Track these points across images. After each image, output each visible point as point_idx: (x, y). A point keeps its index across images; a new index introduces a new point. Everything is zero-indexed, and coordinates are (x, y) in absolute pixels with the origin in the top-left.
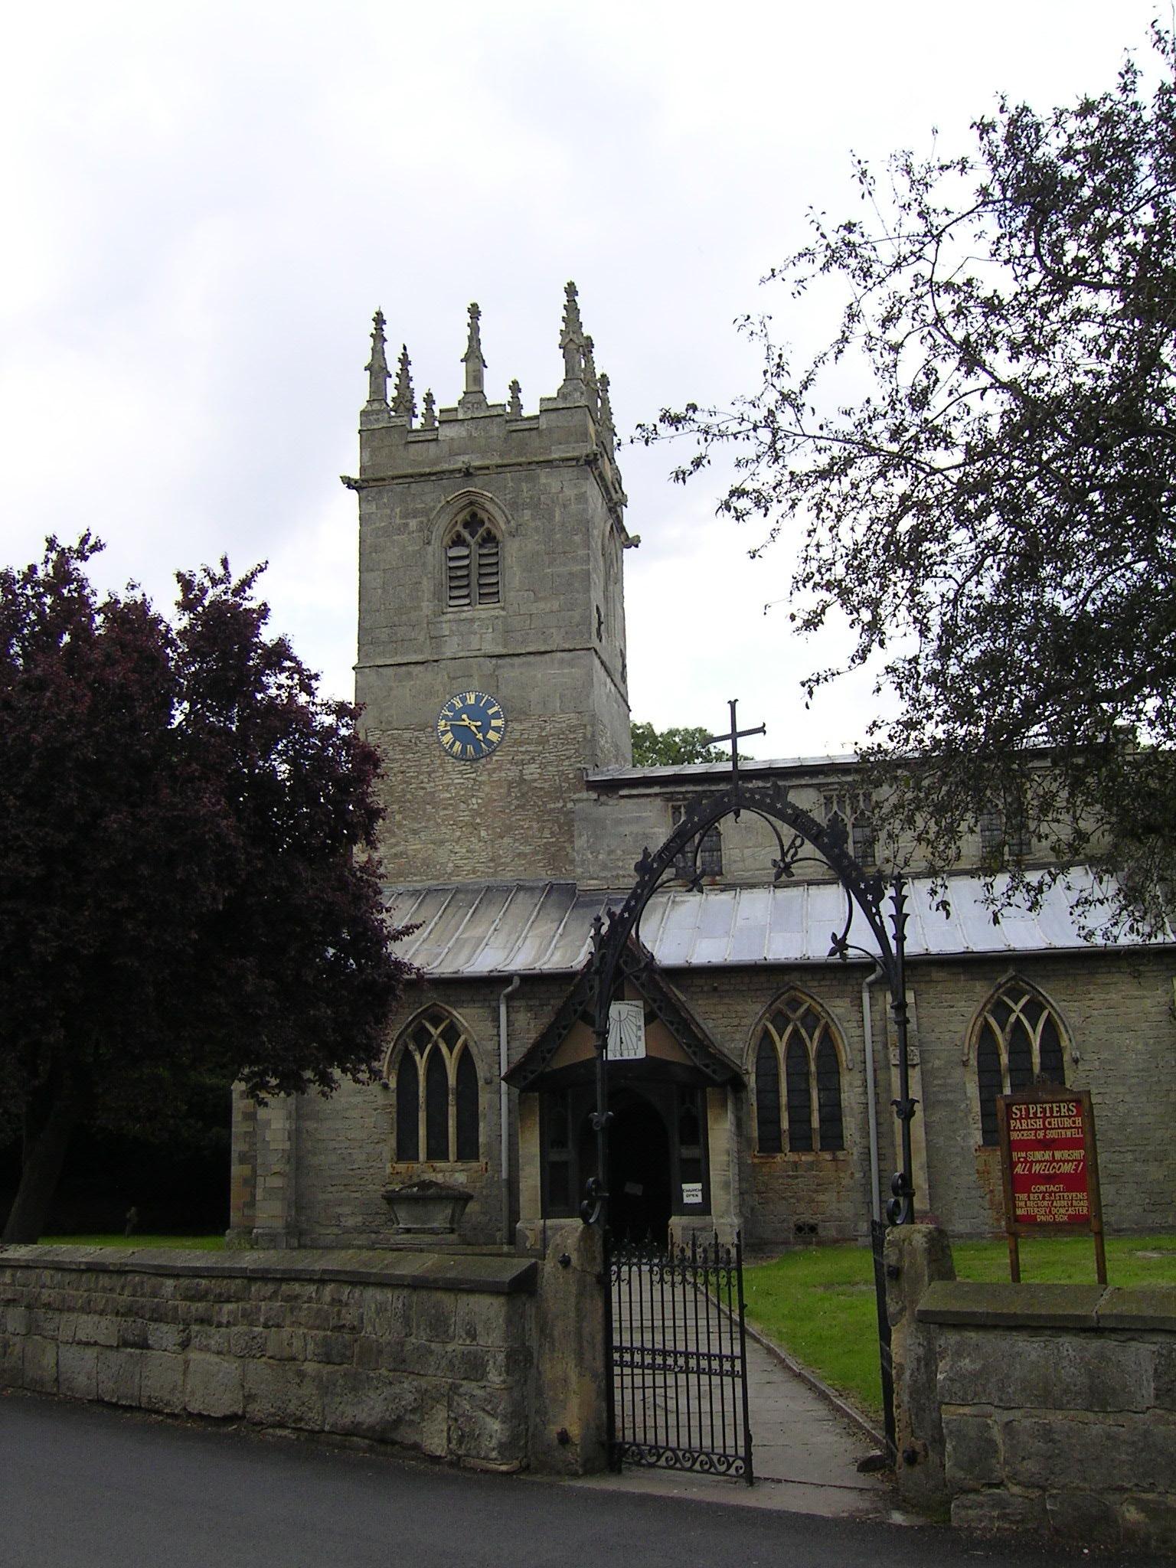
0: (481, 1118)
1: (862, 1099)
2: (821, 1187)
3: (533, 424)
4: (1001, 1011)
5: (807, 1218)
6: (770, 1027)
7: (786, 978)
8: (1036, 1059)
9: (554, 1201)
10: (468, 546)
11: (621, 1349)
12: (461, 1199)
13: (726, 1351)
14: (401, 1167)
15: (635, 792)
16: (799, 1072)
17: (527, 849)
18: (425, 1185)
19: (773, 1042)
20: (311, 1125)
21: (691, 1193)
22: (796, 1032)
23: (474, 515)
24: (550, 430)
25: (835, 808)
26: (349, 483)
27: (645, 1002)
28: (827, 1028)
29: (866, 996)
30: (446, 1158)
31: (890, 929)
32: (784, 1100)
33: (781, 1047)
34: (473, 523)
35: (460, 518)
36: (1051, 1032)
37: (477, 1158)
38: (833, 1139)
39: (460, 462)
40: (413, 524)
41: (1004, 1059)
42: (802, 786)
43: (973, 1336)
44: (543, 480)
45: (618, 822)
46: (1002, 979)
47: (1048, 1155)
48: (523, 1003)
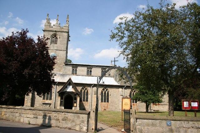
9: (61, 105)
12: (50, 104)
16: (84, 94)
21: (75, 105)
22: (84, 90)
37: (51, 100)
38: (87, 101)
39: (55, 30)
43: (141, 120)
45: (67, 68)
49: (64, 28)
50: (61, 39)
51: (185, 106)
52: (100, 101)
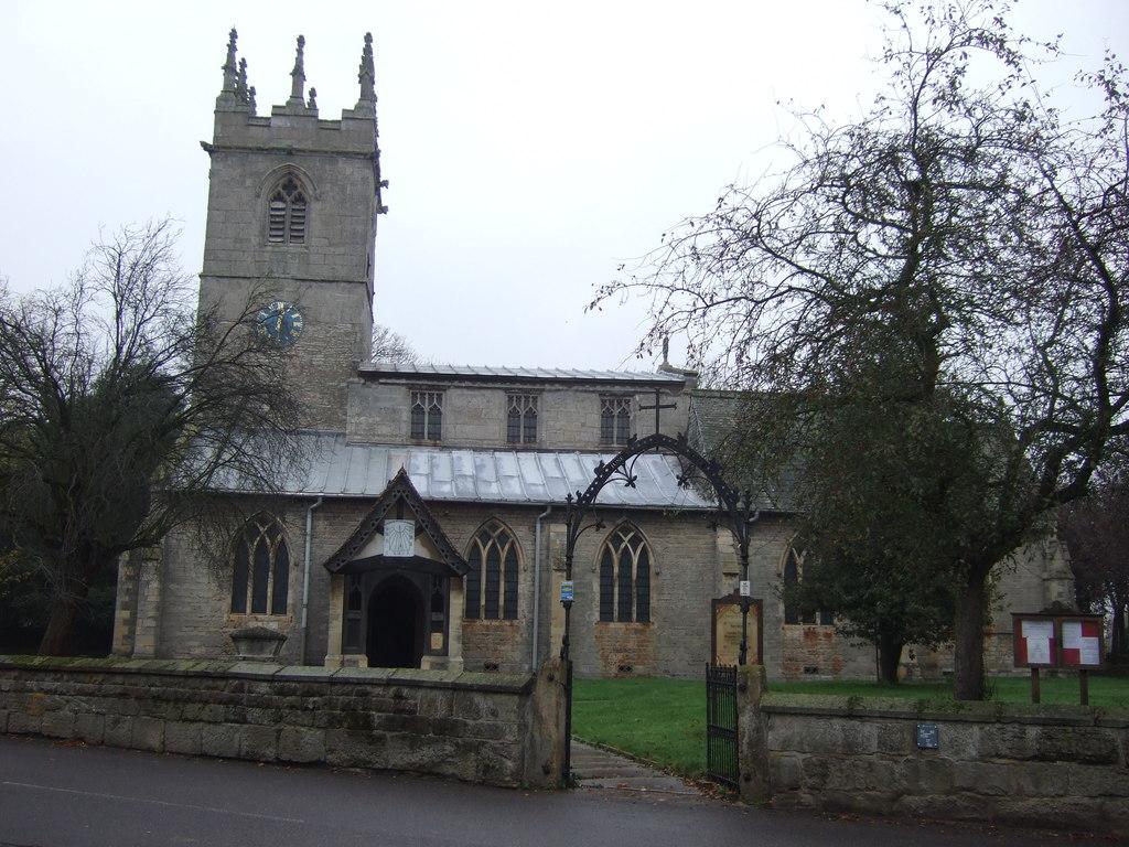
0: (289, 587)
1: (532, 589)
2: (503, 641)
3: (335, 126)
4: (616, 540)
5: (492, 660)
6: (611, 546)
7: (490, 512)
8: (635, 571)
10: (285, 202)
14: (234, 617)
15: (389, 381)
19: (498, 553)
20: (173, 586)
21: (436, 640)
22: (494, 545)
23: (291, 181)
24: (348, 131)
25: (514, 404)
26: (205, 146)
27: (417, 522)
28: (513, 544)
29: (538, 526)
30: (264, 612)
32: (483, 587)
33: (484, 554)
34: (290, 186)
35: (282, 181)
36: (644, 553)
38: (511, 613)
39: (284, 144)
41: (616, 570)
42: (398, 384)
44: (340, 165)
46: (619, 522)
48: (321, 514)
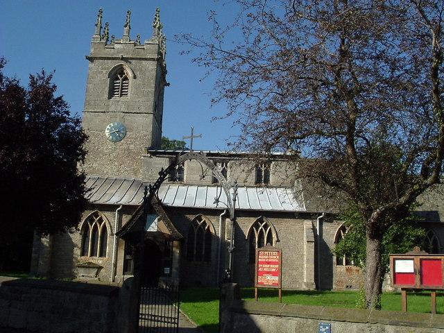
11: (142, 314)
12: (100, 268)
13: (173, 316)
17: (128, 169)
18: (90, 263)
21: (167, 271)
22: (96, 225)
31: (232, 197)
40: (104, 71)
45: (156, 164)
47: (268, 266)
49: (145, 47)
50: (138, 81)
51: (145, 309)
52: (421, 257)
